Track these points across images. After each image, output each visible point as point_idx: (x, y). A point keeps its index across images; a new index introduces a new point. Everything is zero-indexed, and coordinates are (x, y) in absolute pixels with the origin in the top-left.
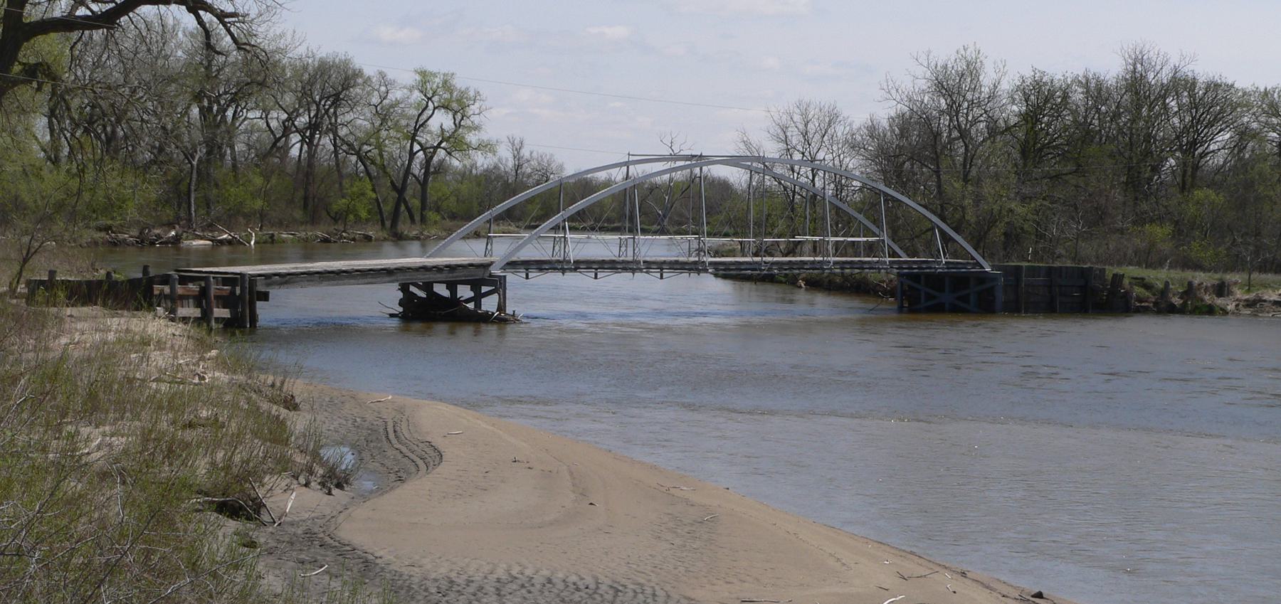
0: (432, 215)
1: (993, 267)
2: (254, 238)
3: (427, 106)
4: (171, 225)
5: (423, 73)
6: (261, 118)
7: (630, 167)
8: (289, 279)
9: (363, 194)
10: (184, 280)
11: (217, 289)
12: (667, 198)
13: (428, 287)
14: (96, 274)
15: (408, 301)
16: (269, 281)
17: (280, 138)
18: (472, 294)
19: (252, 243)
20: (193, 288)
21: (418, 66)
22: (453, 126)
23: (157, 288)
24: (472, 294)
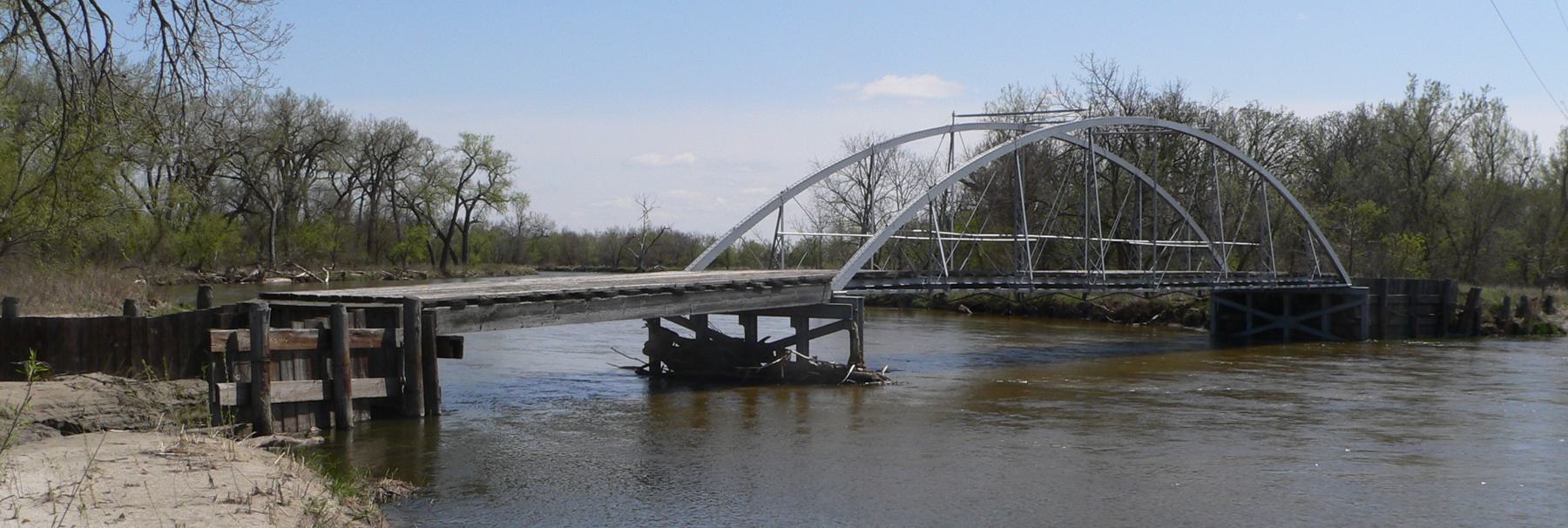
0: (471, 255)
1: (1353, 280)
2: (328, 276)
3: (470, 164)
4: (254, 265)
5: (466, 137)
6: (328, 178)
7: (955, 133)
8: (499, 309)
9: (420, 238)
10: (282, 317)
11: (357, 334)
12: (642, 245)
13: (699, 323)
14: (154, 308)
15: (659, 343)
16: (459, 314)
17: (345, 194)
18: (793, 332)
19: (327, 280)
20: (305, 332)
21: (462, 131)
22: (489, 183)
23: (219, 338)
24: (793, 332)
